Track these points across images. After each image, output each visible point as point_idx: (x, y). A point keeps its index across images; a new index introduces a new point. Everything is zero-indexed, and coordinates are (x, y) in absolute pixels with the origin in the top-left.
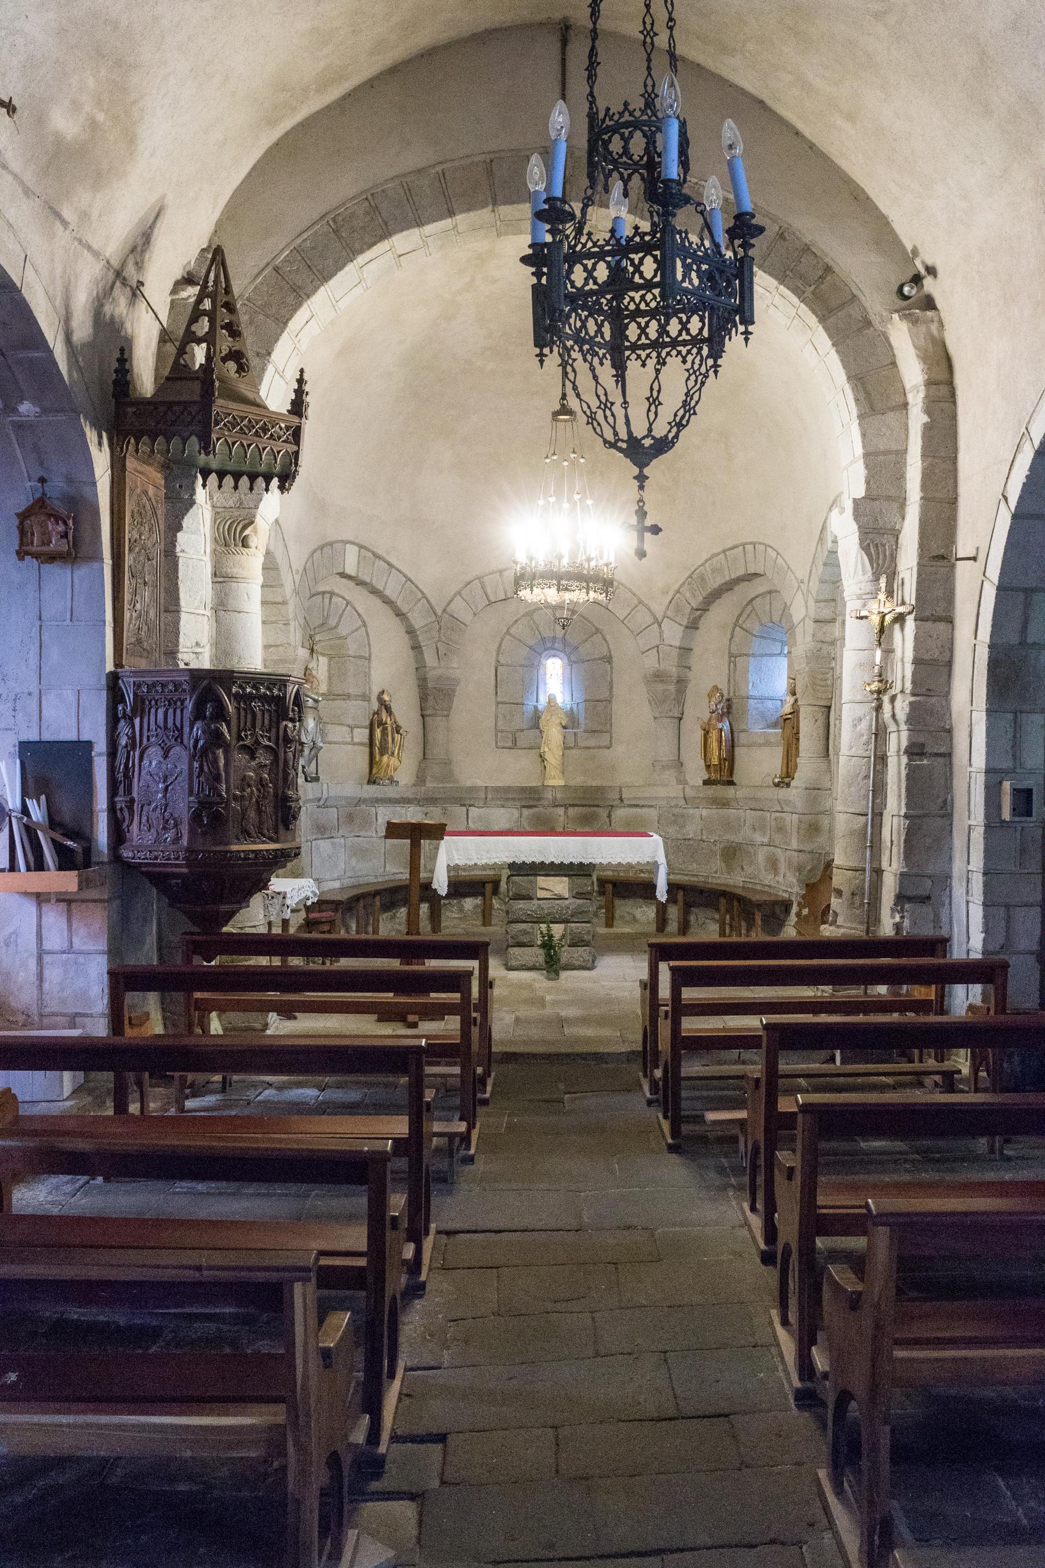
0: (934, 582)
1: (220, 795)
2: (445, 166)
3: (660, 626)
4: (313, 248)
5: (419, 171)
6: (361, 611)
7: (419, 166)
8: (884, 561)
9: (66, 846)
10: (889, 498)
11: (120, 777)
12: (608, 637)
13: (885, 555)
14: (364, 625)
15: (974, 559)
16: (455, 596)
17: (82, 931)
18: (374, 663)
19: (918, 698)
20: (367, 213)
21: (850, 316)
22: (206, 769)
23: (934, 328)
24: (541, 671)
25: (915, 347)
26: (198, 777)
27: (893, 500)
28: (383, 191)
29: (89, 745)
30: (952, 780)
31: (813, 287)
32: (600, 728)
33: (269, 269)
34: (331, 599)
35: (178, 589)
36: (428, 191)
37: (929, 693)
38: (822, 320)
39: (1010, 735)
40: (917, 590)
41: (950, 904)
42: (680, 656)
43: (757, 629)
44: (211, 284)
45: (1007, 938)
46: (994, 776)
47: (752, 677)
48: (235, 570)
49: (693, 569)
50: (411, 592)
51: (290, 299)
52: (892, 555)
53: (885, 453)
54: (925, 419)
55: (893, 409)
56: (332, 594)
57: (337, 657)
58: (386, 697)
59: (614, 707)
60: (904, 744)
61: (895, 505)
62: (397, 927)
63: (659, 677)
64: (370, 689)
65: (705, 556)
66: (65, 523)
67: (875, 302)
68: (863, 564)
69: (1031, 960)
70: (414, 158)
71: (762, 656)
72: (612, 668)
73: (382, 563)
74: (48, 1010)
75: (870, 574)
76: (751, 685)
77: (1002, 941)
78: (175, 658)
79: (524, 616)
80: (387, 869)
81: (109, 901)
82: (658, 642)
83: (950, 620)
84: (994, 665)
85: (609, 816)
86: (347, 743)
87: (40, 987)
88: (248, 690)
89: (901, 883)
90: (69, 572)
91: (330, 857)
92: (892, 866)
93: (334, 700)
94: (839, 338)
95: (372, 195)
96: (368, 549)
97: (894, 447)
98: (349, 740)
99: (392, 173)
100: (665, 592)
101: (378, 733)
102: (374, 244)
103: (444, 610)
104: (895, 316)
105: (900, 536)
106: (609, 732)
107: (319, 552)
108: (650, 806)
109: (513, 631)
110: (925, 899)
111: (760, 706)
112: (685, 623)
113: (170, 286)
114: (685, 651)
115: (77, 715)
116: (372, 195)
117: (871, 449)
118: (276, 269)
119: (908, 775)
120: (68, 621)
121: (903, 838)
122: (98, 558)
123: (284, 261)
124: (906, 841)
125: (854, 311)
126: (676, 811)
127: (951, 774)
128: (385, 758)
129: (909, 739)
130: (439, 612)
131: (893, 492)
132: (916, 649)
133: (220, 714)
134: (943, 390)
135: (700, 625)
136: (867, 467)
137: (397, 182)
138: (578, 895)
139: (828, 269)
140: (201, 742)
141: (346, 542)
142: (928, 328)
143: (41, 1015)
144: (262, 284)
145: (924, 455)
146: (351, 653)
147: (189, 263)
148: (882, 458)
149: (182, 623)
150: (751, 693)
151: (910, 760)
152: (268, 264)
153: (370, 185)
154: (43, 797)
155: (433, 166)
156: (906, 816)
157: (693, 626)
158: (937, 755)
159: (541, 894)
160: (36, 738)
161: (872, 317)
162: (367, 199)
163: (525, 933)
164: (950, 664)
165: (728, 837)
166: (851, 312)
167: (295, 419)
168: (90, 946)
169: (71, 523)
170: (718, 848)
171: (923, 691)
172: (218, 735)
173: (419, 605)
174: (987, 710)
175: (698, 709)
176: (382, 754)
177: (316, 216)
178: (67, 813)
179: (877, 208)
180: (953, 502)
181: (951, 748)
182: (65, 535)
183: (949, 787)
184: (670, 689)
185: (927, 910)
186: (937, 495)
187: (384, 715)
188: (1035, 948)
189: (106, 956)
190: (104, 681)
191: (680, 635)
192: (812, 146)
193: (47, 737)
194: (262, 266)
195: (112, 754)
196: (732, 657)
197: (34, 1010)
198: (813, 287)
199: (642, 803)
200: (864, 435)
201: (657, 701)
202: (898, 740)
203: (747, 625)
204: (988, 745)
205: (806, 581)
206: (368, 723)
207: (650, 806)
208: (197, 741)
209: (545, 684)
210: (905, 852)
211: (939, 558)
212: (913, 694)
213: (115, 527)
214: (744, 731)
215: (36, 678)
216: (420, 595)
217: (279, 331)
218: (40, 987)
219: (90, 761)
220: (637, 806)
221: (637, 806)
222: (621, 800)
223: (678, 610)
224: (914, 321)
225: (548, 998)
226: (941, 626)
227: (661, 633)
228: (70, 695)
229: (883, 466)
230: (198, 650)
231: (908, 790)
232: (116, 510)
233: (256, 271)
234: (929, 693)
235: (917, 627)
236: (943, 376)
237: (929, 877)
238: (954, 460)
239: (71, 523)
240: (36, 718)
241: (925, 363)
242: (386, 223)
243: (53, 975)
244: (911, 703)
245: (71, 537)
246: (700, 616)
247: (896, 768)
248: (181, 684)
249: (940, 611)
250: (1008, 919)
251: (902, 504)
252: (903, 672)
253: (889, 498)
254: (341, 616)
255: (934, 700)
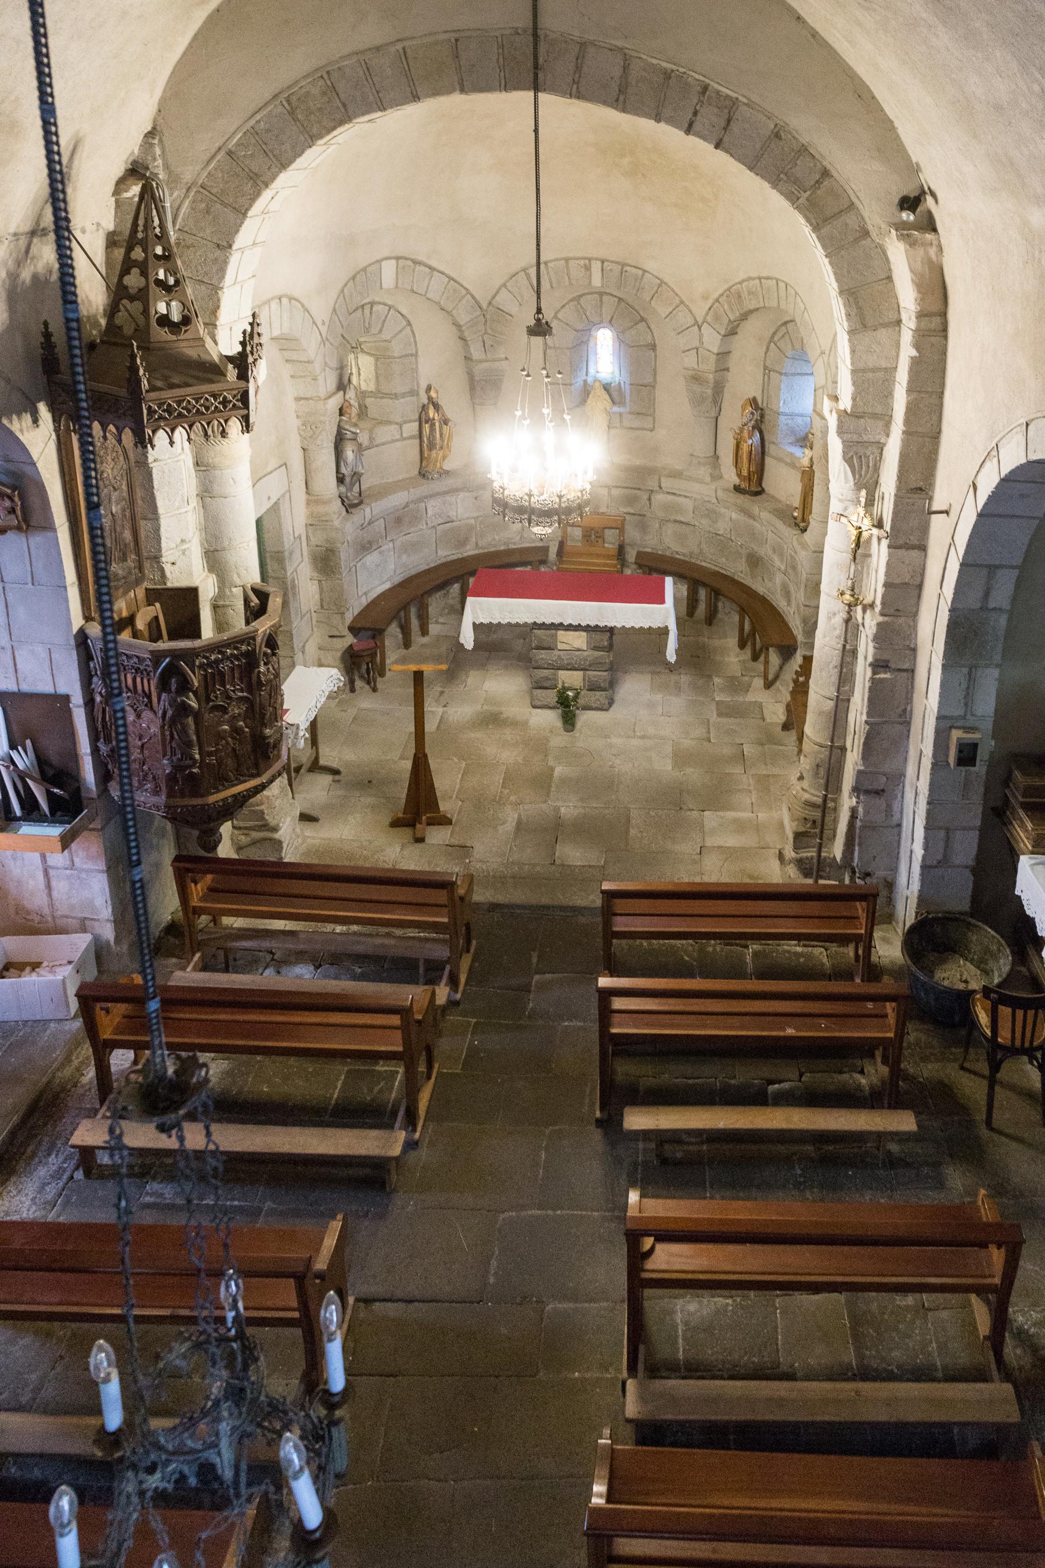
0: (910, 512)
1: (192, 758)
2: (406, 44)
3: (700, 328)
4: (268, 131)
5: (378, 49)
6: (404, 312)
7: (378, 42)
8: (866, 475)
9: (55, 794)
10: (875, 416)
11: (100, 728)
12: (652, 326)
13: (868, 466)
14: (409, 324)
15: (947, 512)
16: (500, 289)
17: (82, 854)
18: (421, 360)
19: (886, 619)
20: (324, 93)
21: (847, 225)
22: (176, 736)
23: (932, 252)
24: (591, 344)
25: (911, 271)
26: (170, 742)
27: (879, 419)
28: (339, 68)
29: (66, 698)
30: (912, 693)
31: (808, 193)
32: (644, 411)
33: (223, 153)
34: (371, 309)
35: (155, 499)
36: (389, 72)
37: (897, 613)
38: (816, 228)
39: (964, 686)
40: (892, 520)
41: (903, 797)
42: (718, 360)
43: (789, 353)
44: (141, 228)
45: (945, 856)
46: (945, 724)
47: (783, 395)
48: (216, 460)
49: (731, 284)
50: (455, 290)
51: (248, 187)
52: (875, 465)
53: (873, 370)
54: (914, 353)
55: (885, 325)
56: (372, 304)
57: (382, 357)
58: (433, 394)
59: (657, 393)
60: (870, 659)
61: (881, 423)
62: (451, 602)
63: (696, 378)
64: (418, 384)
65: (742, 276)
66: (13, 501)
67: (875, 210)
68: (846, 473)
69: (967, 873)
70: (372, 33)
71: (794, 375)
72: (656, 356)
73: (422, 268)
74: (59, 913)
75: (852, 483)
76: (782, 402)
77: (940, 857)
78: (159, 562)
79: (571, 300)
80: (440, 553)
81: (102, 829)
82: (698, 344)
83: (923, 548)
84: (953, 626)
85: (650, 499)
86: (397, 440)
87: (50, 895)
88: (213, 658)
89: (857, 777)
90: (25, 540)
91: (378, 566)
92: (853, 761)
93: (382, 398)
94: (833, 248)
95: (328, 72)
96: (406, 259)
97: (884, 364)
98: (398, 437)
99: (346, 51)
100: (705, 298)
101: (427, 428)
102: (334, 128)
103: (490, 303)
104: (893, 232)
105: (885, 449)
106: (653, 415)
107: (351, 283)
108: (686, 497)
109: (560, 316)
110: (879, 793)
111: (790, 422)
112: (723, 333)
113: (110, 187)
114: (723, 355)
115: (49, 669)
116: (328, 72)
117: (861, 365)
118: (230, 153)
119: (870, 688)
120: (30, 584)
121: (862, 740)
122: (49, 526)
123: (238, 144)
124: (865, 744)
125: (851, 219)
126: (709, 506)
127: (913, 687)
128: (434, 452)
129: (875, 655)
130: (484, 306)
131: (879, 410)
132: (887, 574)
133: (185, 686)
134: (937, 321)
135: (739, 330)
136: (854, 384)
137: (355, 59)
138: (596, 648)
139: (826, 173)
140: (170, 713)
141: (379, 261)
142: (926, 253)
143: (54, 917)
144: (216, 169)
145: (910, 391)
146: (396, 355)
147: (133, 152)
148: (870, 375)
149: (162, 530)
150: (781, 410)
151: (874, 673)
152: (220, 149)
153: (324, 62)
154: (28, 742)
155: (393, 43)
156: (866, 722)
157: (732, 332)
158: (900, 670)
159: (560, 646)
160: (15, 689)
161: (870, 228)
162: (322, 77)
163: (547, 679)
164: (920, 587)
165: (752, 545)
166: (848, 221)
167: (242, 384)
168: (90, 866)
169: (16, 499)
170: (744, 552)
171: (892, 611)
172: (184, 709)
173: (464, 301)
174: (943, 665)
175: (734, 417)
176: (430, 450)
177: (268, 96)
178: (53, 752)
179: (882, 110)
180: (935, 436)
181: (915, 665)
182: (12, 511)
183: (909, 698)
184: (710, 392)
185: (880, 802)
186: (920, 430)
187: (431, 412)
188: (971, 862)
189: (105, 875)
190: (72, 642)
191: (718, 342)
192: (814, 34)
193: (25, 688)
194: (213, 151)
195: (89, 703)
196: (767, 370)
197: (46, 911)
198: (808, 193)
199: (678, 492)
200: (853, 352)
201: (697, 401)
202: (866, 649)
203: (781, 344)
204: (941, 695)
205: (827, 352)
206: (417, 416)
207: (686, 497)
208: (165, 713)
209: (596, 354)
210: (863, 754)
211: (917, 486)
212: (882, 614)
213: (68, 486)
214: (774, 443)
215: (6, 635)
216: (464, 292)
217: (238, 221)
218: (50, 895)
219: (69, 712)
220: (674, 494)
221: (674, 494)
222: (661, 488)
223: (717, 318)
224: (913, 244)
225: (559, 771)
226: (915, 553)
227: (701, 336)
228: (41, 651)
229: (871, 382)
230: (185, 547)
231: (870, 700)
232: (66, 470)
233: (209, 155)
234: (897, 613)
235: (890, 555)
236: (935, 307)
237: (885, 775)
238: (941, 395)
239: (16, 499)
240: (12, 670)
241: (919, 292)
242: (344, 105)
243: (60, 887)
244: (879, 624)
245: (19, 512)
246: (738, 325)
247: (863, 673)
248: (144, 659)
249: (914, 540)
250: (947, 841)
251: (887, 421)
252: (874, 588)
253: (875, 416)
254: (384, 321)
255: (901, 620)
